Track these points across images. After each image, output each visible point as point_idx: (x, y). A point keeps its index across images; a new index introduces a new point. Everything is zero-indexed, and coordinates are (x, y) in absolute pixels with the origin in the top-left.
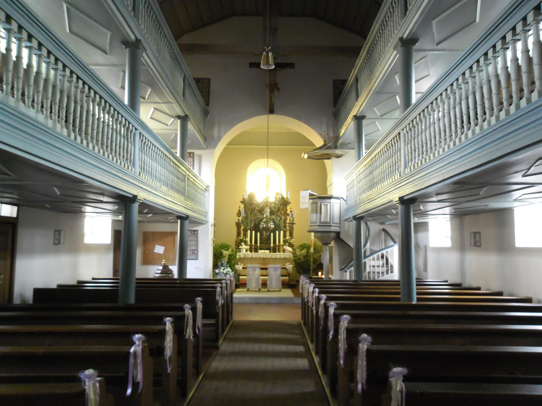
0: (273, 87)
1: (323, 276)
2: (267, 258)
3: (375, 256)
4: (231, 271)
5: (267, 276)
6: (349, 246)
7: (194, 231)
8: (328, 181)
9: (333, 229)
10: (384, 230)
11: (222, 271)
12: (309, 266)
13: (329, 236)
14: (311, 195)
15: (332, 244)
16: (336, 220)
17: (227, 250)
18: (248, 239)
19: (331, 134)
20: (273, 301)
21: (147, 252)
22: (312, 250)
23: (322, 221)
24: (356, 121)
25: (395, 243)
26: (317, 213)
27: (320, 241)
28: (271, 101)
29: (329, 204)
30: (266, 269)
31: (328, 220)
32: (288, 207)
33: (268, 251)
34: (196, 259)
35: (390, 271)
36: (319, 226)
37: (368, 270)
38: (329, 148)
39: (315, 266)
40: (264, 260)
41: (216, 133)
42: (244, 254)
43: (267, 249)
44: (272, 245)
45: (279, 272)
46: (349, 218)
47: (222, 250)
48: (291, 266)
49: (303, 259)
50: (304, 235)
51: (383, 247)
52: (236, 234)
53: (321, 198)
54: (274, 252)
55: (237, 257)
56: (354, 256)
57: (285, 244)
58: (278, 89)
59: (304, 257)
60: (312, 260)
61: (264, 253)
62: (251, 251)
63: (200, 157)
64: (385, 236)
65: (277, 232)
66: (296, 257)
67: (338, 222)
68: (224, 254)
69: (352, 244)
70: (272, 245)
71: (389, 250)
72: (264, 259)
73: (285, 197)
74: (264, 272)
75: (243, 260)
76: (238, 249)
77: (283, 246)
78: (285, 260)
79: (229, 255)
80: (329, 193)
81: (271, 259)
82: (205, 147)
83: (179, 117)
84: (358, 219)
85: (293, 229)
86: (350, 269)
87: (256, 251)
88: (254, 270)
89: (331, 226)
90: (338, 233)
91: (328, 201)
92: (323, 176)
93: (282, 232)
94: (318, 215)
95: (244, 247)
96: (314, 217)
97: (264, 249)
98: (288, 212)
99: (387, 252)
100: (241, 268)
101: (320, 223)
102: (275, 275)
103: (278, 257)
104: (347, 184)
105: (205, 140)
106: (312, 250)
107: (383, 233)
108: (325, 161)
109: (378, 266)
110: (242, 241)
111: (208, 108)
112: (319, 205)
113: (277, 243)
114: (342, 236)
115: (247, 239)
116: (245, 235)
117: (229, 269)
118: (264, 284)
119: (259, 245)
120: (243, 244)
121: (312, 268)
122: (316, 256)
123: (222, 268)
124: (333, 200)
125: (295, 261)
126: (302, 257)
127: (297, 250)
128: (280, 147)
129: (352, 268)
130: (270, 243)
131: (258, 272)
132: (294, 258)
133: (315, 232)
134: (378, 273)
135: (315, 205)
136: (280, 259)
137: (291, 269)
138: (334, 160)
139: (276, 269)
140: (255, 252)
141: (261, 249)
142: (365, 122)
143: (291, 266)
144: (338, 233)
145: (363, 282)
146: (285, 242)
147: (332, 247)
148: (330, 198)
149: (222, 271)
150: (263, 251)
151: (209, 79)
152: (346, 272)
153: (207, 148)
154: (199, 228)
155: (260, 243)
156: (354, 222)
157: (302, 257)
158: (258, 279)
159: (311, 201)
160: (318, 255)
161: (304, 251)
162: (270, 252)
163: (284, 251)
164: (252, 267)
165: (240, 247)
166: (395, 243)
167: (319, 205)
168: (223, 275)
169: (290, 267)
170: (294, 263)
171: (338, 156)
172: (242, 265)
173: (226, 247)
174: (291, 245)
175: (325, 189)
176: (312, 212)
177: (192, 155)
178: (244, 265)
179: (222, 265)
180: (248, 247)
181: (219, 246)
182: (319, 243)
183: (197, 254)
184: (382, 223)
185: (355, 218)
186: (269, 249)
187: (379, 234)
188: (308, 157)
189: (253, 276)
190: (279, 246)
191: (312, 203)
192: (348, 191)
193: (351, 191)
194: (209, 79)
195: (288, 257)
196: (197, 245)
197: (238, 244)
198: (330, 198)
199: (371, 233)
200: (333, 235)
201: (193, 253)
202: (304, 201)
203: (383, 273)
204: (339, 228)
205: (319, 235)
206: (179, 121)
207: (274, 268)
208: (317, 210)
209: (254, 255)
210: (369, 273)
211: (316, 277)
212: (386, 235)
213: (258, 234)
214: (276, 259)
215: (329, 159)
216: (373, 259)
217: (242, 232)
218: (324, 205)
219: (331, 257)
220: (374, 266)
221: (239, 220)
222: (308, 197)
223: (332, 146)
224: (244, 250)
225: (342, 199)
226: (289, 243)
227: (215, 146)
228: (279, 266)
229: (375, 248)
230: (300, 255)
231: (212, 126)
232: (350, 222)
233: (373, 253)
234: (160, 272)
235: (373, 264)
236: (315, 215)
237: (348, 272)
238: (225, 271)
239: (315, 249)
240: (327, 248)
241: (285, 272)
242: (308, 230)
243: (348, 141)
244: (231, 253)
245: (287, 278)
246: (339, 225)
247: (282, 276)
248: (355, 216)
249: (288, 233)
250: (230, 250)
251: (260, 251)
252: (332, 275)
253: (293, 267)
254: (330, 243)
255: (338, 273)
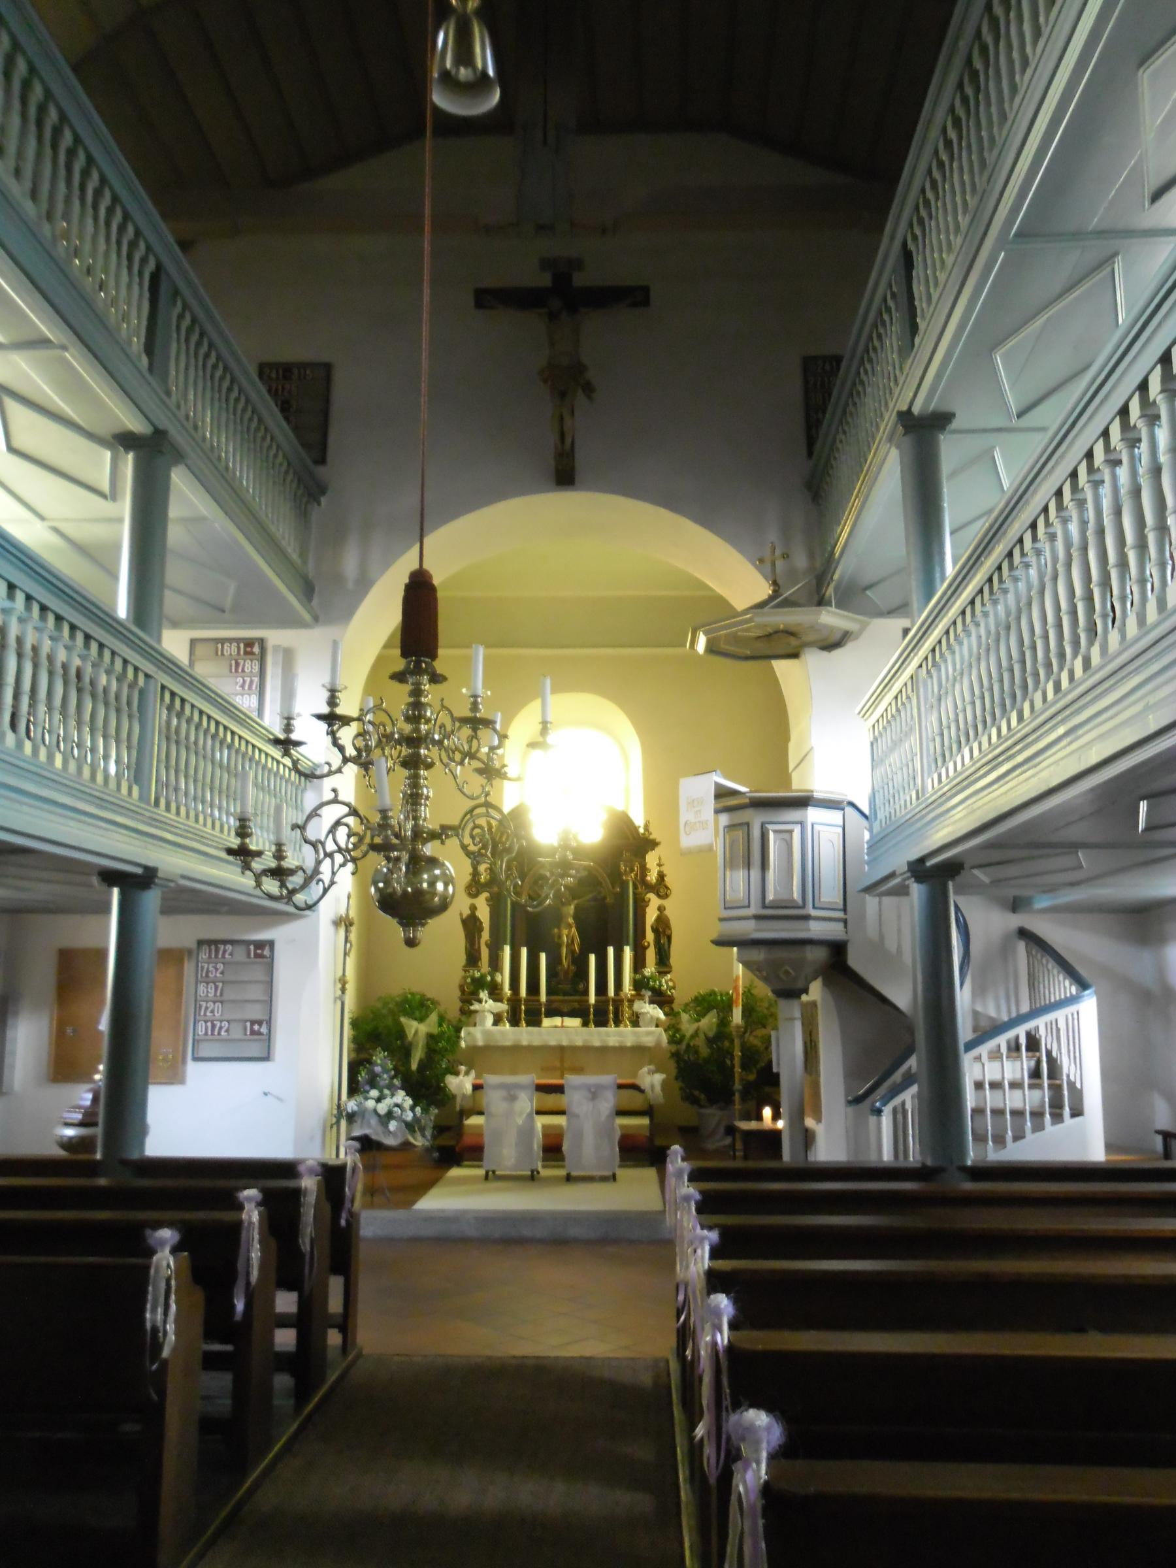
0: (567, 382)
1: (780, 1124)
2: (574, 1049)
3: (1002, 1040)
4: (409, 1102)
5: (562, 1113)
6: (884, 1000)
7: (260, 945)
8: (792, 746)
9: (816, 929)
10: (1023, 933)
11: (370, 1104)
12: (728, 1073)
13: (806, 959)
14: (722, 793)
15: (816, 991)
16: (830, 893)
17: (421, 1020)
18: (504, 978)
19: (801, 561)
20: (573, 1232)
21: (69, 1031)
22: (737, 1016)
23: (770, 896)
24: (908, 441)
25: (1083, 985)
26: (748, 865)
27: (766, 980)
28: (562, 436)
29: (797, 830)
30: (559, 1089)
31: (796, 895)
32: (651, 859)
33: (575, 1022)
34: (267, 1058)
35: (1067, 1111)
36: (758, 917)
37: (970, 1099)
38: (788, 603)
39: (752, 1077)
40: (565, 1057)
41: (350, 564)
42: (487, 1033)
43: (572, 1014)
44: (592, 999)
45: (607, 1103)
46: (892, 875)
47: (403, 1020)
48: (658, 1078)
49: (705, 1051)
50: (706, 964)
51: (1025, 1008)
52: (462, 959)
53: (764, 805)
54: (597, 1025)
55: (463, 1044)
56: (915, 1045)
57: (639, 996)
58: (589, 389)
59: (710, 1041)
60: (738, 1053)
61: (561, 1030)
62: (515, 1022)
63: (288, 655)
64: (1029, 953)
65: (611, 950)
66: (679, 1042)
67: (839, 900)
68: (410, 1034)
69: (903, 994)
70: (592, 999)
71: (1060, 1015)
72: (561, 1050)
73: (639, 821)
74: (551, 1100)
75: (480, 1057)
76: (467, 1015)
77: (631, 1001)
78: (639, 1051)
79: (430, 1037)
80: (799, 784)
81: (587, 1049)
82: (307, 617)
83: (125, 440)
84: (938, 874)
85: (669, 938)
86: (897, 1101)
87: (534, 1020)
88: (512, 1098)
89: (807, 918)
90: (838, 949)
91: (794, 815)
92: (774, 726)
93: (628, 952)
94: (755, 873)
95: (488, 1006)
96: (738, 883)
97: (562, 1014)
98: (652, 877)
99: (1054, 1028)
100: (468, 1088)
101: (764, 906)
102: (592, 1117)
103: (613, 1041)
104: (871, 749)
105: (308, 590)
106: (737, 1016)
107: (1021, 946)
108: (781, 667)
109: (1015, 1085)
110: (479, 984)
111: (321, 471)
112: (756, 833)
113: (611, 992)
114: (854, 961)
115: (499, 978)
116: (495, 965)
117: (401, 1097)
118: (553, 1150)
119: (543, 997)
120: (484, 995)
121: (737, 1086)
122: (754, 1040)
123: (374, 1093)
124: (813, 814)
125: (676, 1055)
126: (700, 1042)
127: (685, 1017)
128: (621, 643)
129: (908, 1097)
130: (586, 992)
131: (526, 1103)
132: (674, 1048)
133: (744, 944)
134: (1017, 1114)
135: (740, 834)
136: (621, 1050)
137: (658, 1089)
138: (813, 659)
139: (594, 1093)
140: (530, 1023)
141: (551, 1013)
142: (951, 451)
143: (658, 1078)
144: (838, 949)
145: (968, 1186)
146: (639, 985)
147: (814, 1004)
148: (803, 802)
149: (370, 1104)
150: (557, 1021)
151: (328, 367)
152: (879, 1112)
153: (316, 619)
154: (279, 934)
155: (549, 992)
156: (917, 891)
157: (700, 1042)
158: (526, 1132)
159: (724, 819)
160: (761, 1032)
161: (709, 1022)
162: (585, 1024)
163: (636, 1021)
164: (504, 1086)
165: (476, 1006)
166: (1083, 985)
167: (756, 833)
168: (374, 1121)
169: (653, 1080)
170: (672, 1065)
171: (832, 643)
172: (473, 1074)
173: (419, 1006)
174: (661, 999)
175: (784, 777)
176: (730, 863)
177: (256, 649)
178: (478, 1077)
179: (373, 1083)
180: (503, 1007)
181: (397, 1004)
182: (763, 990)
183: (269, 1040)
184: (1016, 905)
185: (919, 869)
186: (580, 1012)
187: (1005, 951)
188: (711, 649)
189: (508, 1116)
190: (618, 1003)
191: (731, 827)
192: (875, 763)
193: (894, 758)
194: (328, 367)
195: (649, 1041)
196: (269, 1002)
197: (469, 995)
198: (803, 802)
199: (976, 947)
200: (818, 955)
201: (253, 1032)
202: (698, 825)
203: (1037, 1115)
204: (841, 926)
205: (758, 955)
206: (130, 456)
207: (588, 1088)
208: (749, 853)
209: (525, 1035)
210: (978, 1112)
211: (753, 1125)
212: (1038, 953)
213: (543, 957)
214: (604, 1050)
215: (795, 655)
216: (995, 1055)
217: (485, 953)
218: (783, 837)
219: (811, 1046)
220: (995, 1085)
221: (473, 908)
222: (710, 803)
223: (812, 599)
224: (490, 1020)
225: (849, 810)
226: (653, 990)
227: (345, 614)
228: (608, 1079)
229: (994, 1009)
230: (696, 1034)
231: (336, 537)
232: (888, 901)
233: (987, 1031)
234: (79, 1116)
235: (997, 1077)
236: (741, 874)
237: (887, 1110)
238: (382, 1108)
239: (748, 1011)
240: (792, 1010)
241: (633, 1100)
242: (714, 936)
243: (869, 576)
244: (435, 1030)
245: (645, 1121)
246: (840, 915)
247: (621, 1113)
248: (922, 860)
249: (651, 955)
250: (433, 1017)
251: (547, 1022)
252: (819, 1120)
253: (664, 1084)
254: (806, 991)
255: (841, 1129)
